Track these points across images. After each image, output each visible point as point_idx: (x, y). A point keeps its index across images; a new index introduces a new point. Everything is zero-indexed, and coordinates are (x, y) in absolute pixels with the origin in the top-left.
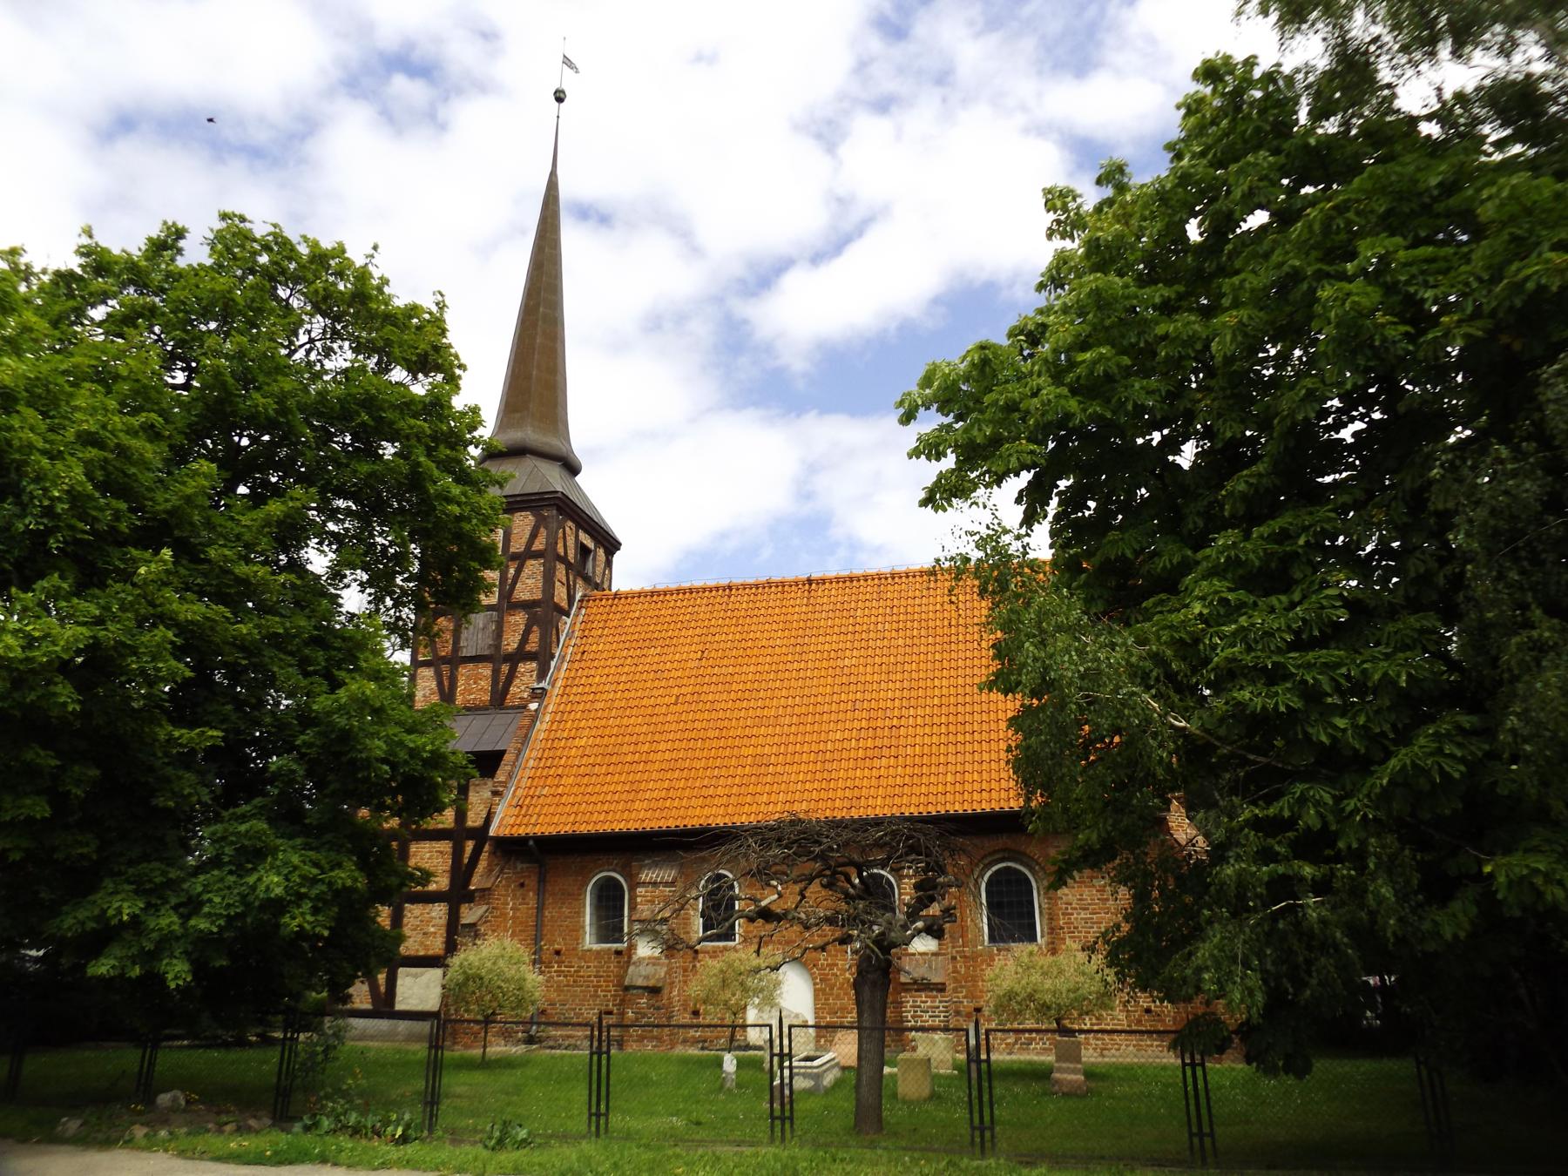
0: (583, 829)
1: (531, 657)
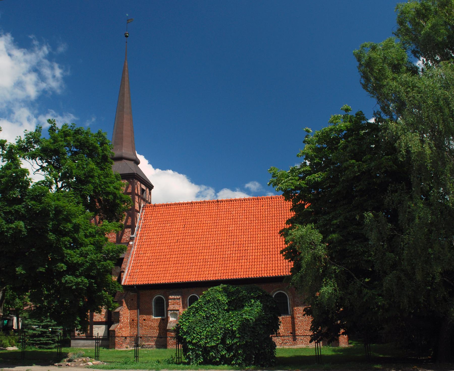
0: (152, 282)
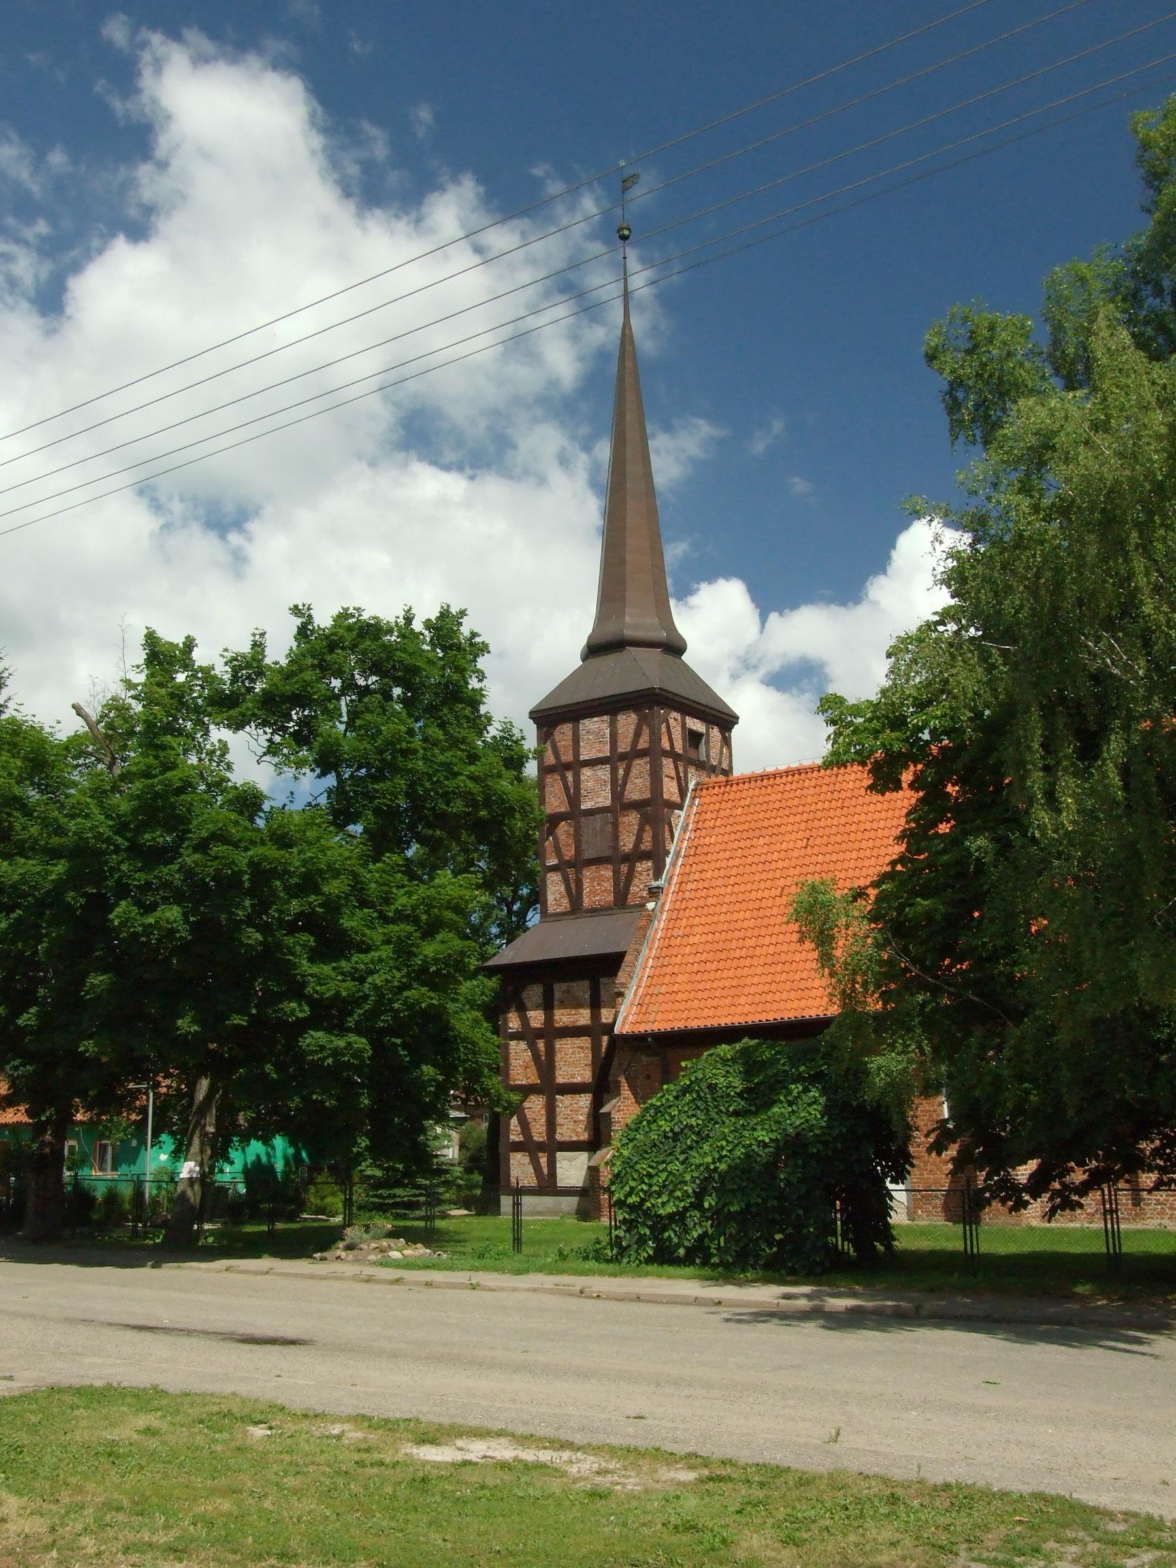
0: (694, 1024)
1: (646, 856)
